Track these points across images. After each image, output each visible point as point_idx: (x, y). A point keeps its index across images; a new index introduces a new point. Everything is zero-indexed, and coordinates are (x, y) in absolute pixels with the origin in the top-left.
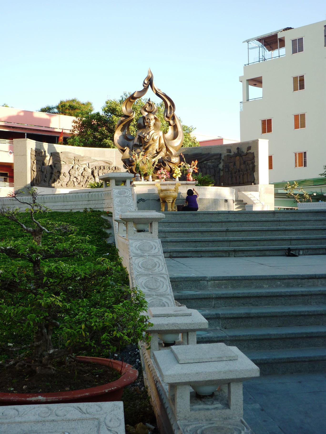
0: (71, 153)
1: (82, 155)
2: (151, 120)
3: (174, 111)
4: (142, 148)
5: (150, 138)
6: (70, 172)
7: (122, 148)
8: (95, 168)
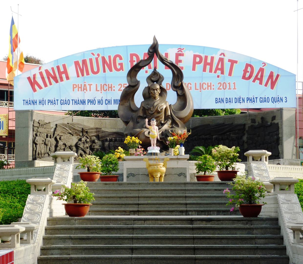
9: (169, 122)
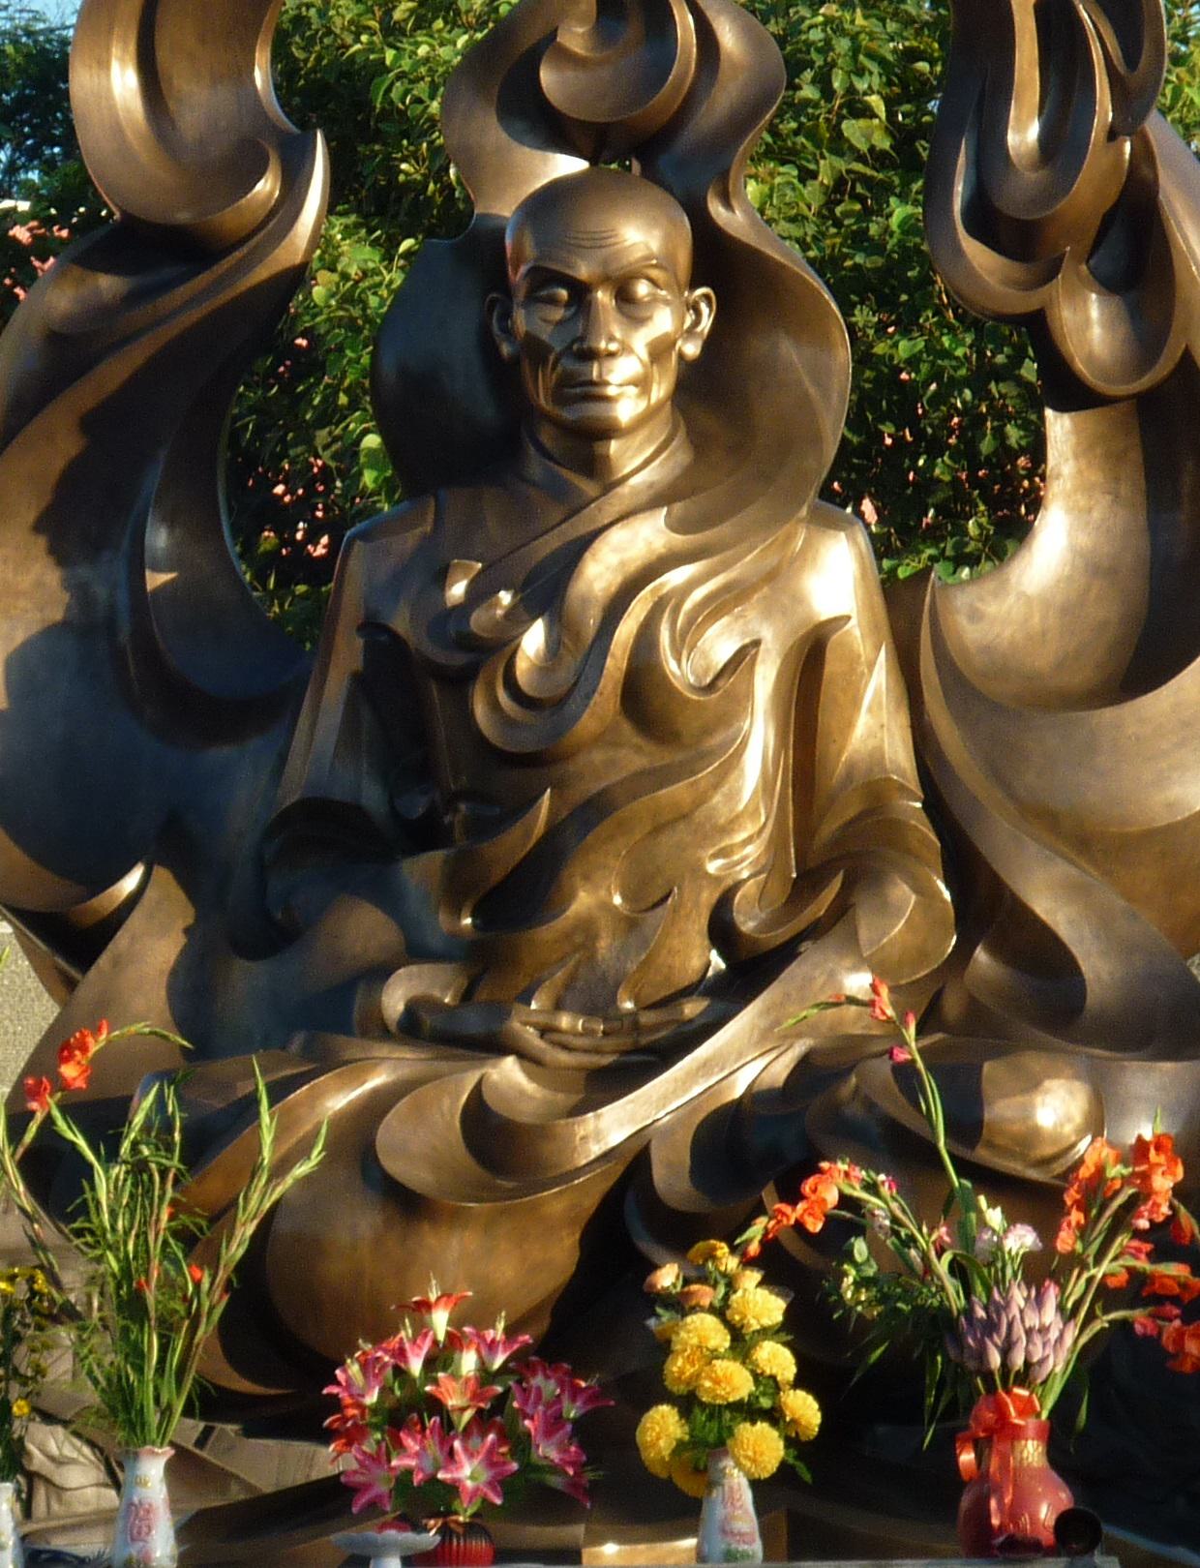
2: (603, 297)
3: (1133, 103)
4: (421, 871)
5: (570, 663)
7: (46, 889)
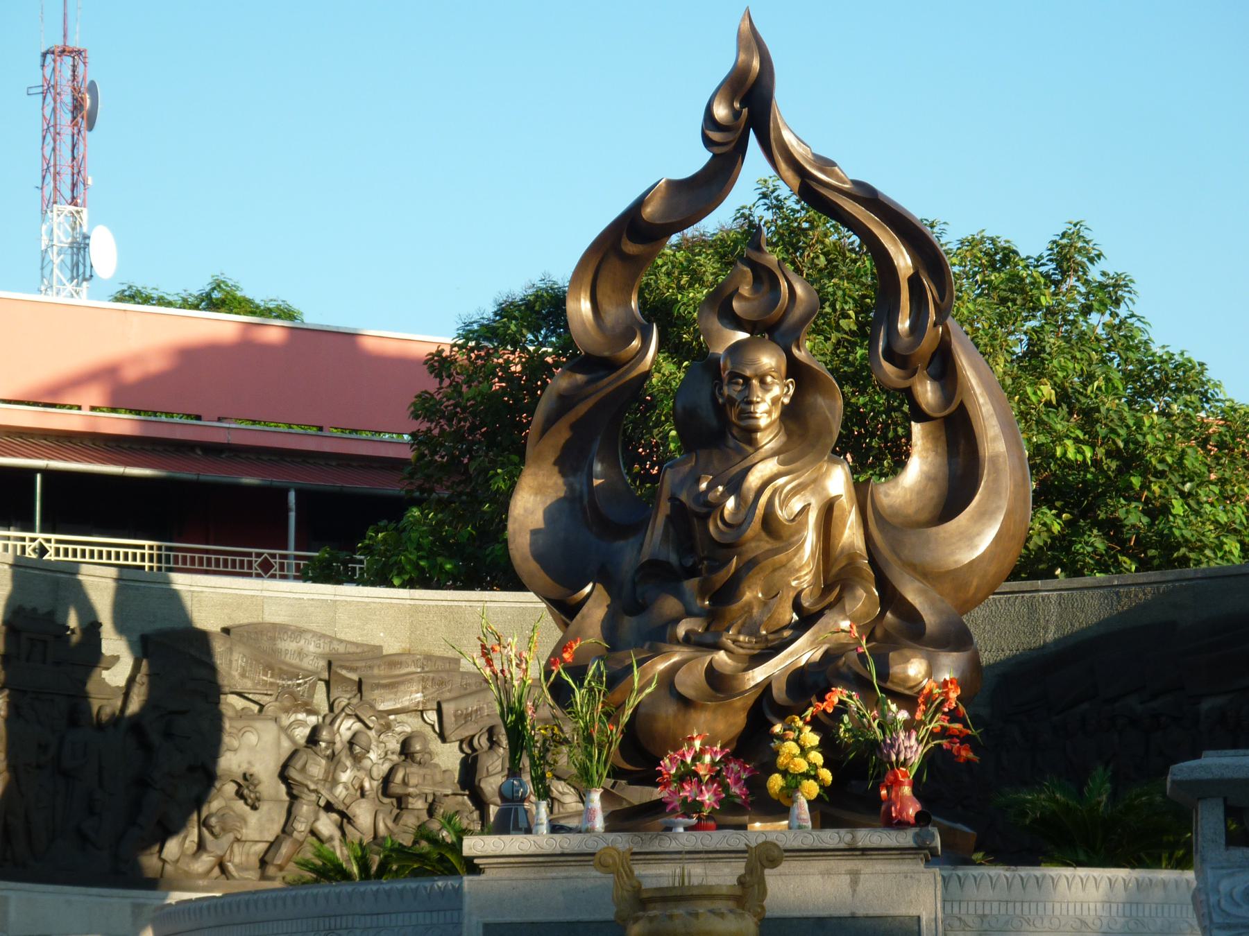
0: (299, 633)
1: (392, 646)
2: (755, 382)
4: (691, 585)
6: (293, 773)
8: (490, 739)
9: (864, 598)
